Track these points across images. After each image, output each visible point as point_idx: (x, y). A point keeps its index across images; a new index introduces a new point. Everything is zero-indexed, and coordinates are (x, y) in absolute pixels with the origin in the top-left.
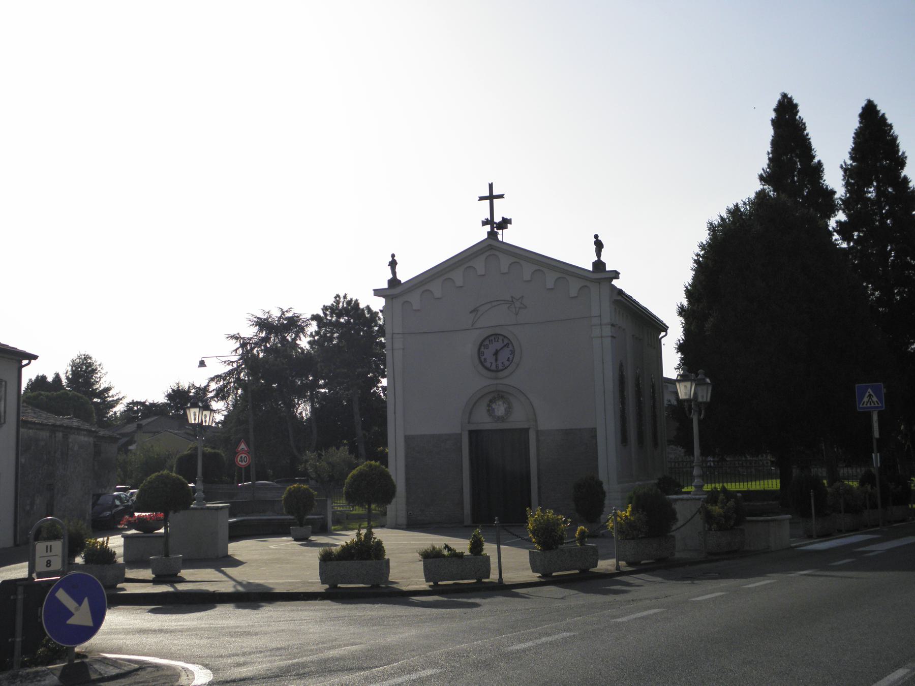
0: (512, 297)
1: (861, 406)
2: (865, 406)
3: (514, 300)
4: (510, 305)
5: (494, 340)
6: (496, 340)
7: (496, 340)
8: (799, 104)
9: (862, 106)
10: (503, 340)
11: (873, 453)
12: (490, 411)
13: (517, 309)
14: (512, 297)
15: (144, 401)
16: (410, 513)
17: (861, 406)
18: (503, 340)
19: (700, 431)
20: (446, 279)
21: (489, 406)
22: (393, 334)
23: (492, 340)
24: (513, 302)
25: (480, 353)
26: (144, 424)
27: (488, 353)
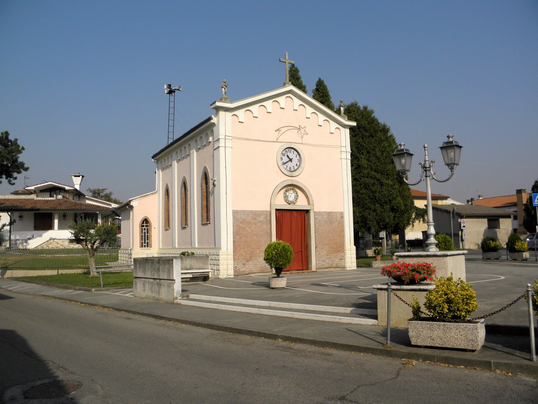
0: (299, 126)
1: (534, 204)
2: (536, 203)
3: (300, 128)
4: (298, 131)
5: (288, 151)
6: (290, 151)
7: (290, 151)
8: (7, 130)
9: (10, 135)
10: (293, 152)
11: (537, 225)
12: (286, 197)
13: (303, 134)
14: (299, 126)
15: (440, 148)
16: (236, 266)
17: (534, 204)
18: (293, 152)
19: (138, 196)
20: (287, 97)
21: (285, 194)
22: (225, 136)
23: (287, 151)
24: (300, 129)
25: (300, 160)
26: (176, 296)
27: (295, 160)
